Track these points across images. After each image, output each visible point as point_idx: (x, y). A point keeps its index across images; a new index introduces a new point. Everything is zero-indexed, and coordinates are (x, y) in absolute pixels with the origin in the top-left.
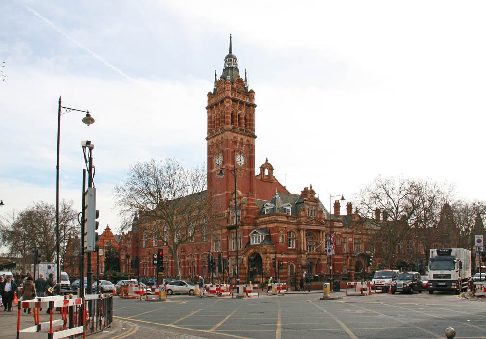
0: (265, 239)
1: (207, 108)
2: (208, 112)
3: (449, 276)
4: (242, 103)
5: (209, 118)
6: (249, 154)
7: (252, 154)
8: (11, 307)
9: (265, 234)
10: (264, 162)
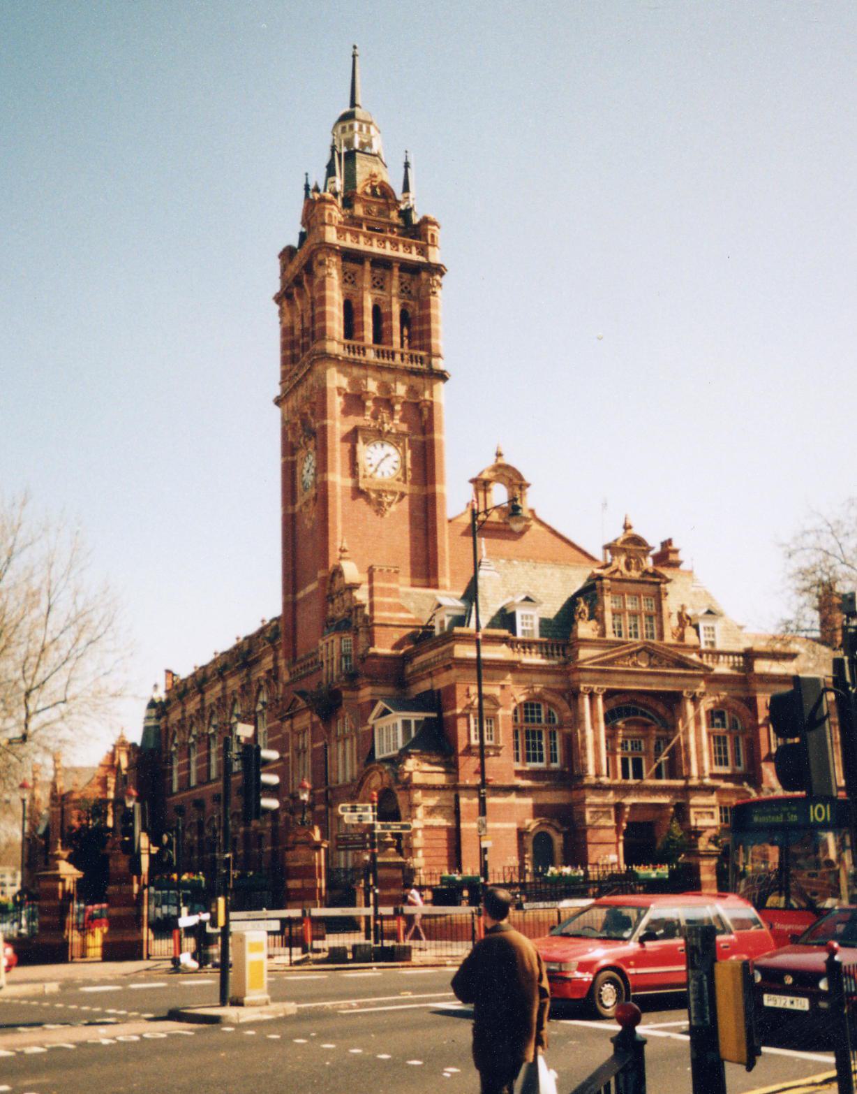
0: (418, 736)
1: (278, 299)
2: (281, 313)
3: (320, 877)
4: (382, 263)
5: (287, 332)
6: (420, 438)
7: (428, 436)
8: (714, 960)
9: (421, 716)
10: (491, 461)
